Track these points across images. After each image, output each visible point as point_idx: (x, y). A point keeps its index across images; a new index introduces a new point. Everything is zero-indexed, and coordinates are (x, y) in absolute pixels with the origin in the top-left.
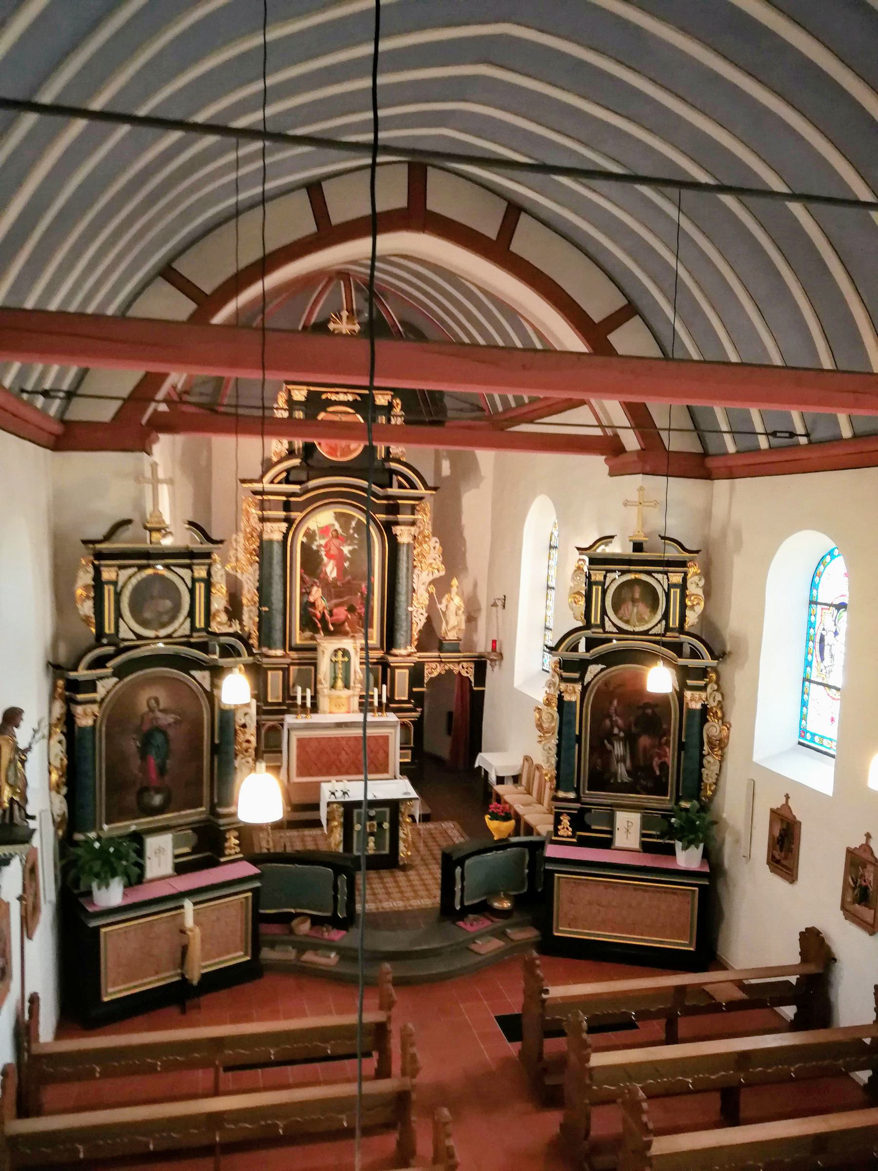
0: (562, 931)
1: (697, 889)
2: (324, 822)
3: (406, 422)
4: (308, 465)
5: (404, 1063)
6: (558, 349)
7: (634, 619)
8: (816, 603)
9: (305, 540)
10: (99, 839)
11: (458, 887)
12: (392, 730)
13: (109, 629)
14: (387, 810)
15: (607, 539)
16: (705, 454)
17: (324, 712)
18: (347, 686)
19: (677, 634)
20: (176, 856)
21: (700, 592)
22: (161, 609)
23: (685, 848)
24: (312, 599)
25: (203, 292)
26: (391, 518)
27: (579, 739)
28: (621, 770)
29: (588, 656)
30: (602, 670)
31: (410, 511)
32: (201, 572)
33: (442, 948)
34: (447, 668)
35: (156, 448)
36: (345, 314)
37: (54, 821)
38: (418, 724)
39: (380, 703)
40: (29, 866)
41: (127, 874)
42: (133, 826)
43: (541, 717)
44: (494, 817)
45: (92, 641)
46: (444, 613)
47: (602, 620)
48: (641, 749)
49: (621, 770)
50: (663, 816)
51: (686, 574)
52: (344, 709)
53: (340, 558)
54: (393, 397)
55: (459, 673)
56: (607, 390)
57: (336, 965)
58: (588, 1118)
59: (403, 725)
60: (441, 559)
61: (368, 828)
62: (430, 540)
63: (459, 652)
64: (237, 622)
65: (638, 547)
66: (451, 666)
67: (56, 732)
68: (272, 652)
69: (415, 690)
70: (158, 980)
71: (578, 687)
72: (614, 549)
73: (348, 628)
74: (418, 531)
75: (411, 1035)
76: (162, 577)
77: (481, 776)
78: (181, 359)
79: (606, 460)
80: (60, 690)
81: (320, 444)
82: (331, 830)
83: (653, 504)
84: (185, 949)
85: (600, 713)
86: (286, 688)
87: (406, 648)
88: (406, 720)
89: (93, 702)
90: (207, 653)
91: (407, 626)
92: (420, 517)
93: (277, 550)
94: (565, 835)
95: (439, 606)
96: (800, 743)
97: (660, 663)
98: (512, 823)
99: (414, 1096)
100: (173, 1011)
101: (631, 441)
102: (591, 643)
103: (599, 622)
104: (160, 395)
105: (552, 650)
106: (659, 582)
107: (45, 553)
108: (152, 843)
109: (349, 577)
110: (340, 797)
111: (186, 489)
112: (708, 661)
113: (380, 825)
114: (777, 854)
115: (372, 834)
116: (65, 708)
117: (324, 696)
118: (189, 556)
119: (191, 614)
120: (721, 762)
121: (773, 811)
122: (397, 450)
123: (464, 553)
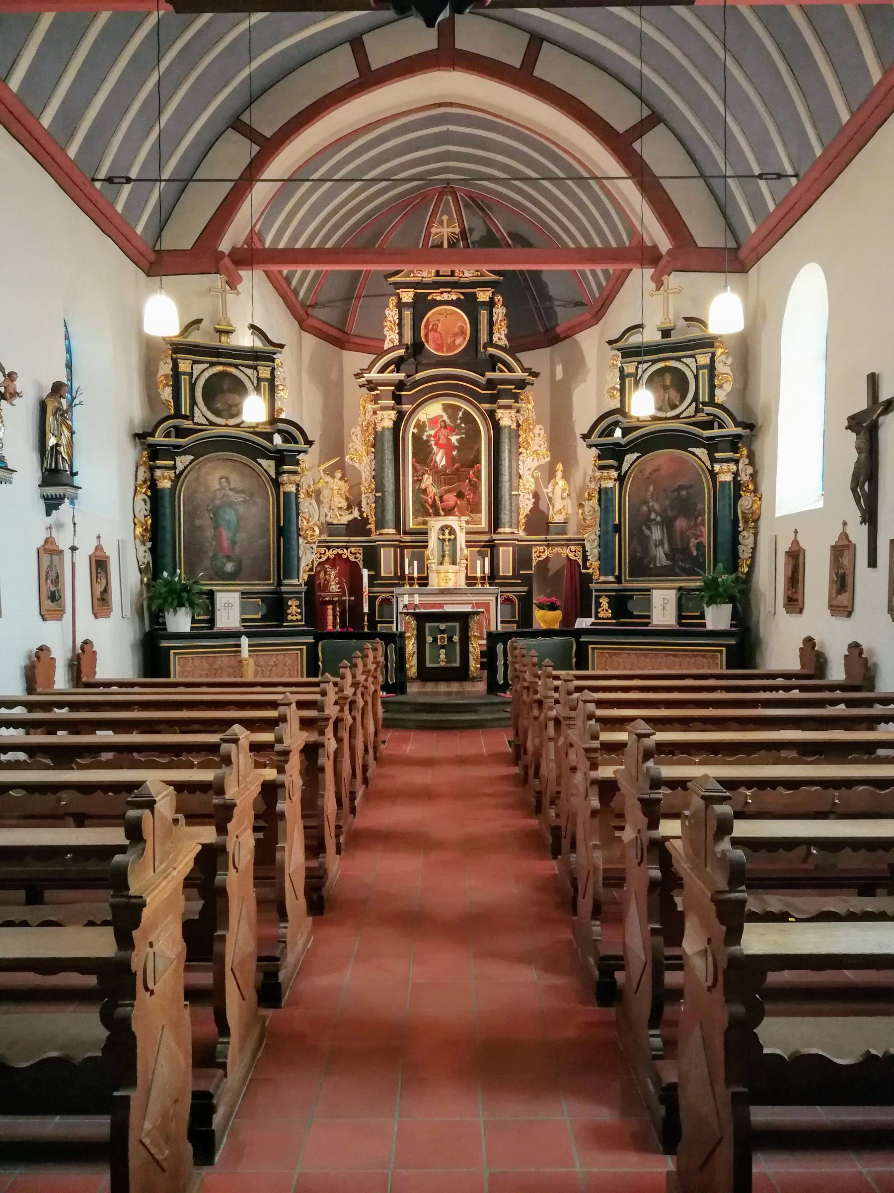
1: (724, 648)
9: (415, 431)
24: (423, 486)
25: (265, 136)
28: (660, 555)
29: (623, 441)
30: (638, 458)
37: (140, 569)
46: (550, 499)
49: (660, 555)
51: (713, 355)
55: (567, 556)
60: (546, 445)
62: (534, 427)
65: (666, 333)
66: (558, 549)
68: (385, 531)
69: (522, 572)
71: (614, 474)
83: (677, 290)
88: (510, 594)
94: (605, 617)
106: (688, 366)
113: (450, 639)
115: (443, 647)
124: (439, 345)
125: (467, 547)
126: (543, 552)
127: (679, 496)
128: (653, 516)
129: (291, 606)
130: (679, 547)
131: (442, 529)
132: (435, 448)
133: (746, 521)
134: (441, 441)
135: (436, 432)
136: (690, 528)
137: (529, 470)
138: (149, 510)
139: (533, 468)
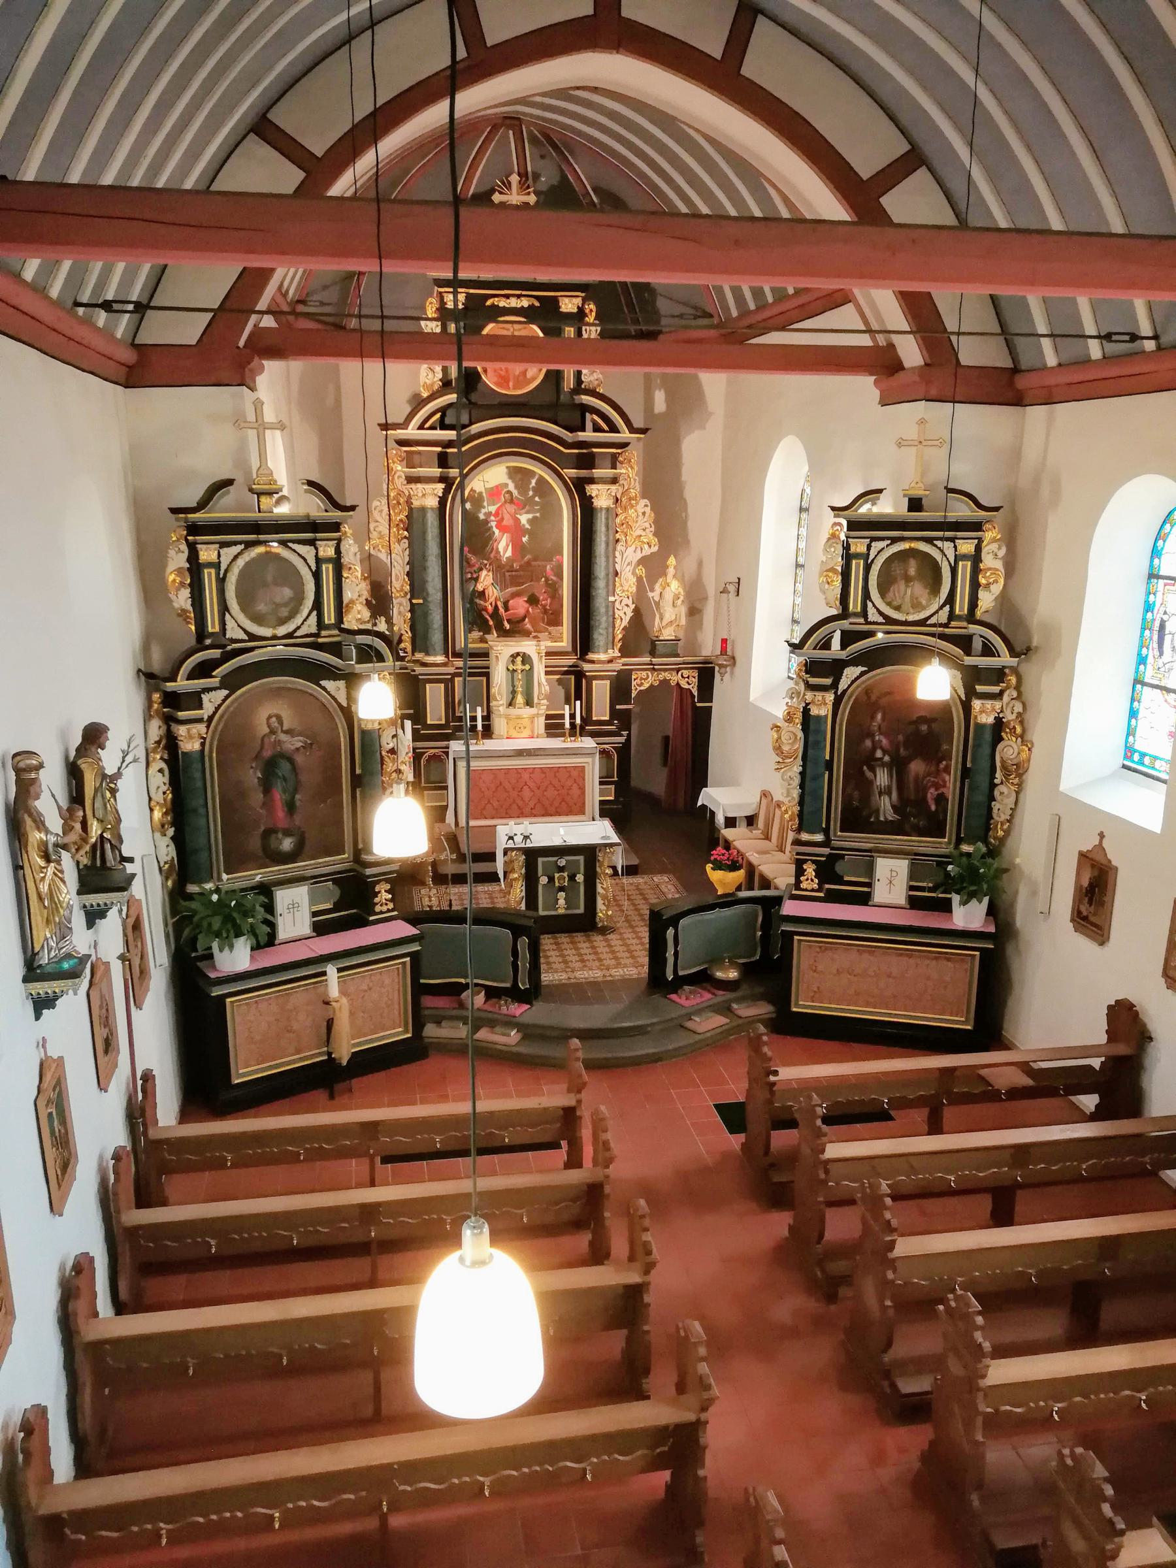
0: (802, 1004)
1: (978, 953)
2: (501, 876)
3: (603, 335)
4: (470, 402)
5: (595, 1151)
6: (808, 217)
7: (907, 605)
8: (1158, 577)
10: (217, 890)
11: (670, 954)
12: (589, 760)
13: (213, 626)
14: (581, 859)
15: (872, 494)
16: (1016, 370)
17: (500, 737)
18: (529, 703)
19: (964, 624)
20: (315, 914)
21: (999, 565)
22: (278, 600)
23: (964, 903)
24: (480, 587)
26: (583, 473)
27: (829, 765)
28: (886, 807)
29: (843, 655)
30: (862, 674)
31: (609, 463)
32: (327, 550)
33: (652, 1024)
34: (661, 677)
35: (262, 381)
36: (514, 179)
38: (624, 751)
39: (573, 725)
40: (131, 921)
41: (253, 932)
42: (258, 876)
43: (779, 738)
44: (718, 866)
45: (192, 641)
46: (657, 604)
47: (864, 607)
48: (911, 779)
49: (886, 807)
50: (939, 864)
51: (980, 540)
52: (527, 733)
53: (516, 531)
54: (584, 300)
55: (678, 684)
56: (876, 274)
57: (517, 1044)
58: (822, 1221)
59: (603, 753)
60: (653, 529)
61: (556, 881)
62: (637, 504)
63: (677, 656)
64: (383, 619)
65: (915, 504)
66: (667, 675)
67: (154, 759)
68: (430, 659)
69: (618, 707)
70: (301, 1059)
71: (830, 697)
72: (887, 507)
73: (529, 626)
74: (621, 490)
75: (603, 1119)
76: (277, 557)
77: (706, 815)
78: (286, 249)
79: (876, 382)
80: (156, 706)
81: (485, 371)
82: (510, 886)
83: (937, 443)
84: (330, 1024)
85: (858, 732)
86: (450, 704)
87: (606, 652)
89: (199, 720)
90: (340, 656)
91: (607, 621)
92: (623, 471)
93: (432, 520)
94: (809, 887)
95: (650, 594)
96: (1124, 767)
97: (936, 661)
98: (741, 874)
99: (607, 1189)
100: (321, 1095)
101: (911, 352)
102: (848, 638)
103: (859, 609)
104: (262, 305)
105: (795, 647)
107: (125, 526)
108: (283, 897)
109: (528, 557)
110: (519, 841)
111: (309, 443)
112: (1005, 659)
113: (572, 878)
114: (1084, 909)
115: (561, 889)
116: (164, 728)
117: (500, 716)
118: (310, 529)
119: (318, 605)
120: (1017, 793)
121: (1083, 855)
122: (591, 376)
123: (685, 522)
124: (500, 376)
125: (547, 673)
126: (645, 679)
127: (918, 731)
128: (879, 754)
129: (379, 892)
130: (912, 797)
131: (514, 657)
132: (497, 532)
133: (1007, 774)
134: (505, 523)
135: (498, 509)
136: (929, 774)
137: (628, 564)
138: (167, 782)
139: (635, 561)
